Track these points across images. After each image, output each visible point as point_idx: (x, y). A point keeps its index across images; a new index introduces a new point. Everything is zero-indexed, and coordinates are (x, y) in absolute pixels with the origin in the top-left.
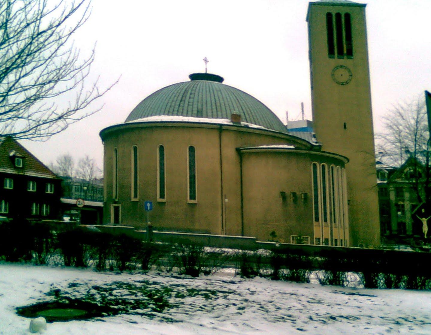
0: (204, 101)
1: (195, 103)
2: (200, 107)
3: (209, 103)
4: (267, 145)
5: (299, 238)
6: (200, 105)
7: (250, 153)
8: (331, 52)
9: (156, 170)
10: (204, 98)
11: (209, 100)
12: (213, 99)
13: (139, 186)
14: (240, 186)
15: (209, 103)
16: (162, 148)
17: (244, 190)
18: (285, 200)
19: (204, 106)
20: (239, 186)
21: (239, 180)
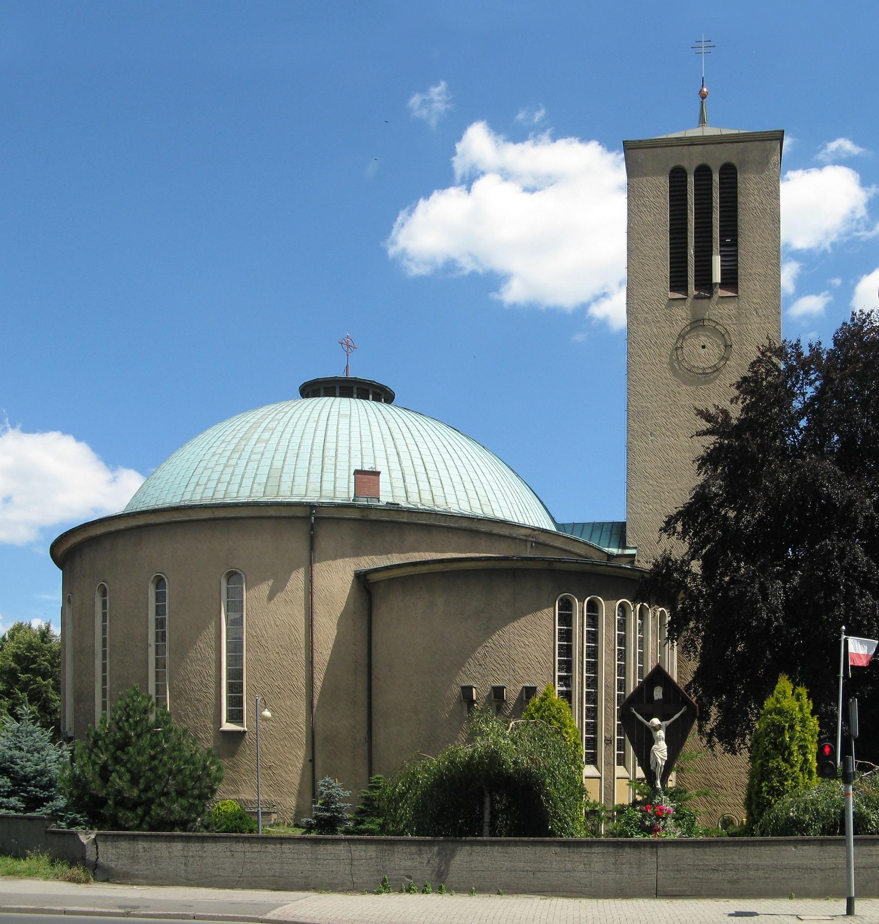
0: (294, 446)
1: (269, 455)
2: (278, 464)
3: (305, 455)
4: (442, 552)
5: (527, 751)
6: (279, 457)
7: (391, 581)
8: (678, 282)
9: (147, 646)
10: (296, 440)
11: (307, 442)
12: (319, 440)
13: (111, 692)
14: (365, 679)
15: (305, 455)
16: (159, 582)
17: (374, 691)
18: (549, 177)
19: (291, 460)
20: (363, 679)
21: (364, 661)
